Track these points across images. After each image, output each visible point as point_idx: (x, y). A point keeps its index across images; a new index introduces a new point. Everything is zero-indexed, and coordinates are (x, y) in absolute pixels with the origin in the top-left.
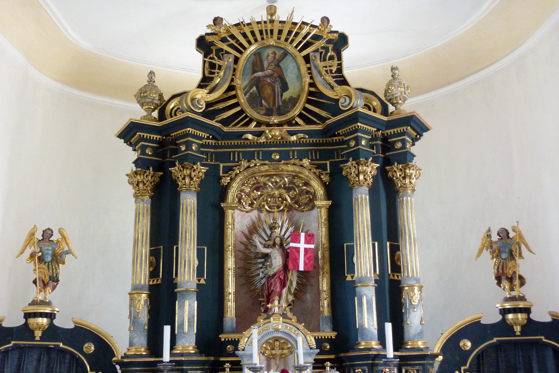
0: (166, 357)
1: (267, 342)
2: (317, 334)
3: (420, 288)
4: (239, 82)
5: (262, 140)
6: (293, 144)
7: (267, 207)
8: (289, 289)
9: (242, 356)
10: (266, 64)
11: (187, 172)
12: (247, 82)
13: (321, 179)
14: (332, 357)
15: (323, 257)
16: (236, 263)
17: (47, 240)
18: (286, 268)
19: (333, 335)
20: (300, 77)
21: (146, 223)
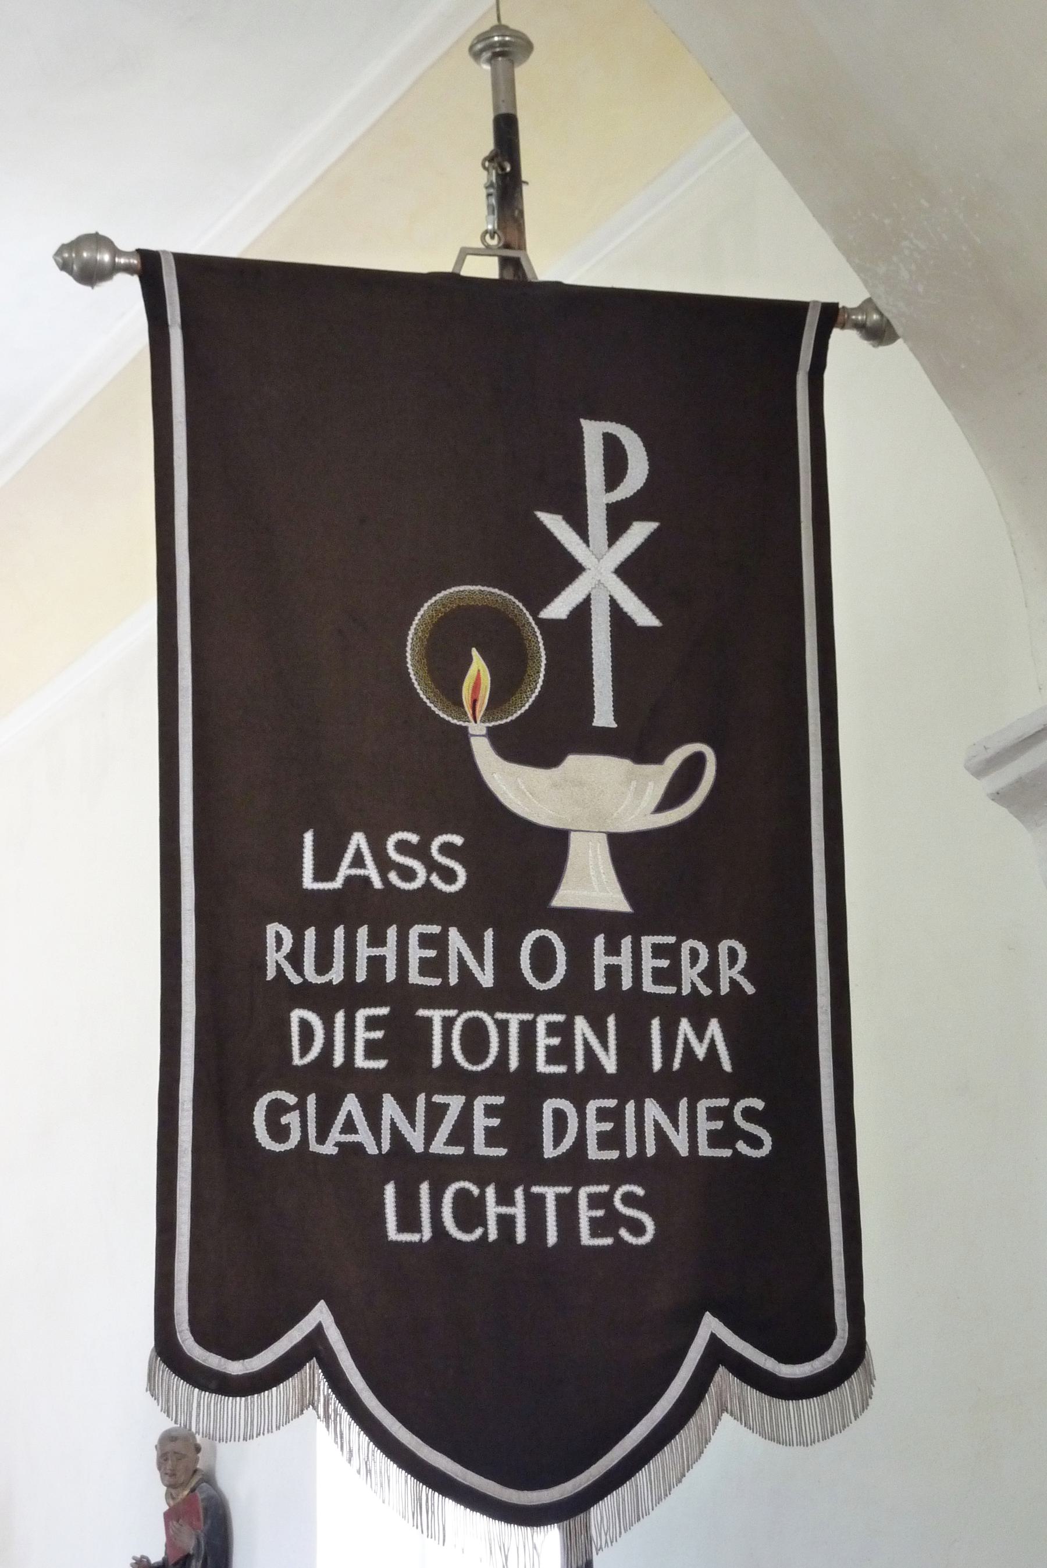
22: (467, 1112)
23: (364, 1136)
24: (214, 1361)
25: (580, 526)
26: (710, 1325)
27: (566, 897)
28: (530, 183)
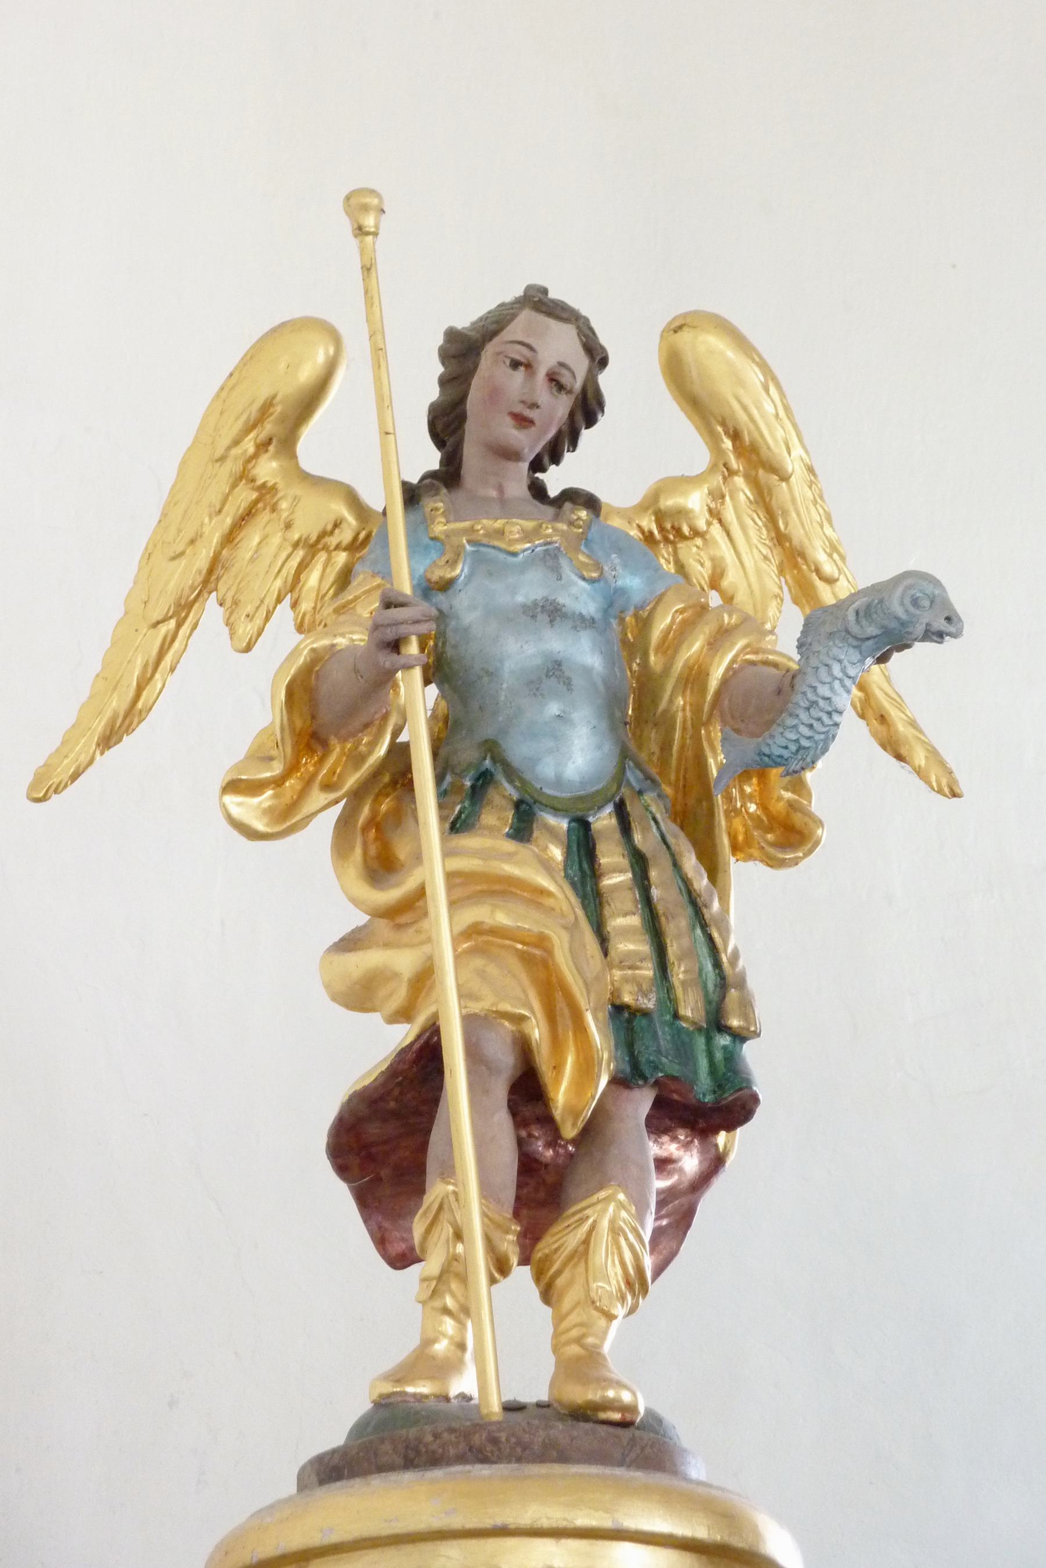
17: (517, 486)
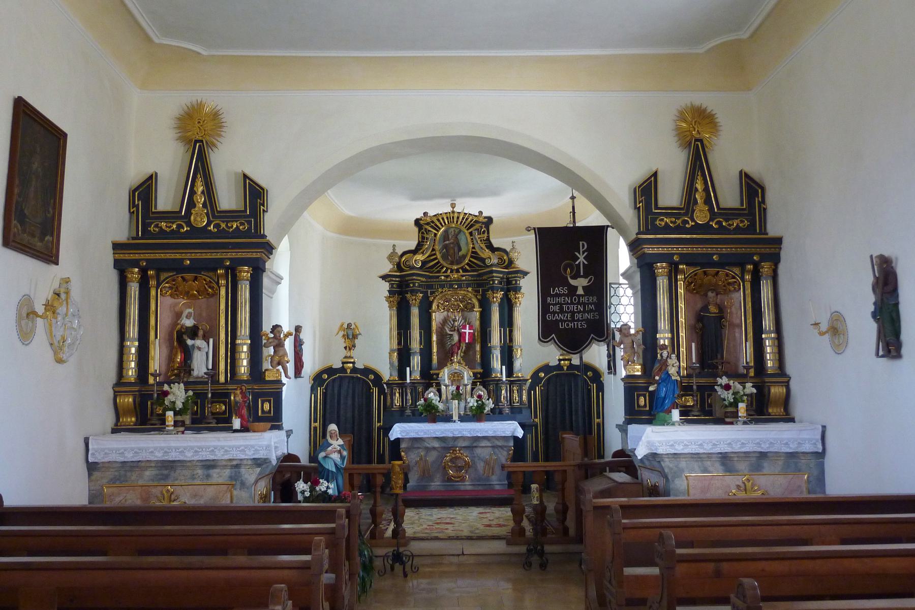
0: (408, 381)
1: (451, 374)
2: (474, 371)
3: (521, 350)
4: (437, 247)
5: (449, 279)
6: (464, 281)
7: (452, 310)
8: (462, 350)
9: (441, 380)
10: (450, 237)
11: (414, 297)
12: (441, 246)
13: (477, 298)
14: (481, 380)
15: (478, 335)
16: (437, 338)
18: (460, 341)
19: (481, 371)
20: (467, 244)
21: (395, 320)
22: (567, 315)
23: (558, 318)
24: (543, 340)
25: (579, 254)
26: (592, 335)
27: (578, 293)
28: (871, 254)
